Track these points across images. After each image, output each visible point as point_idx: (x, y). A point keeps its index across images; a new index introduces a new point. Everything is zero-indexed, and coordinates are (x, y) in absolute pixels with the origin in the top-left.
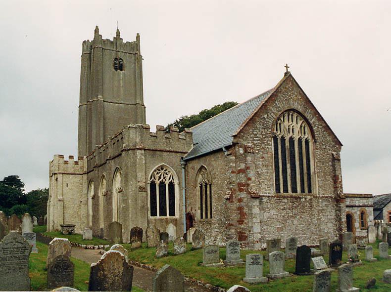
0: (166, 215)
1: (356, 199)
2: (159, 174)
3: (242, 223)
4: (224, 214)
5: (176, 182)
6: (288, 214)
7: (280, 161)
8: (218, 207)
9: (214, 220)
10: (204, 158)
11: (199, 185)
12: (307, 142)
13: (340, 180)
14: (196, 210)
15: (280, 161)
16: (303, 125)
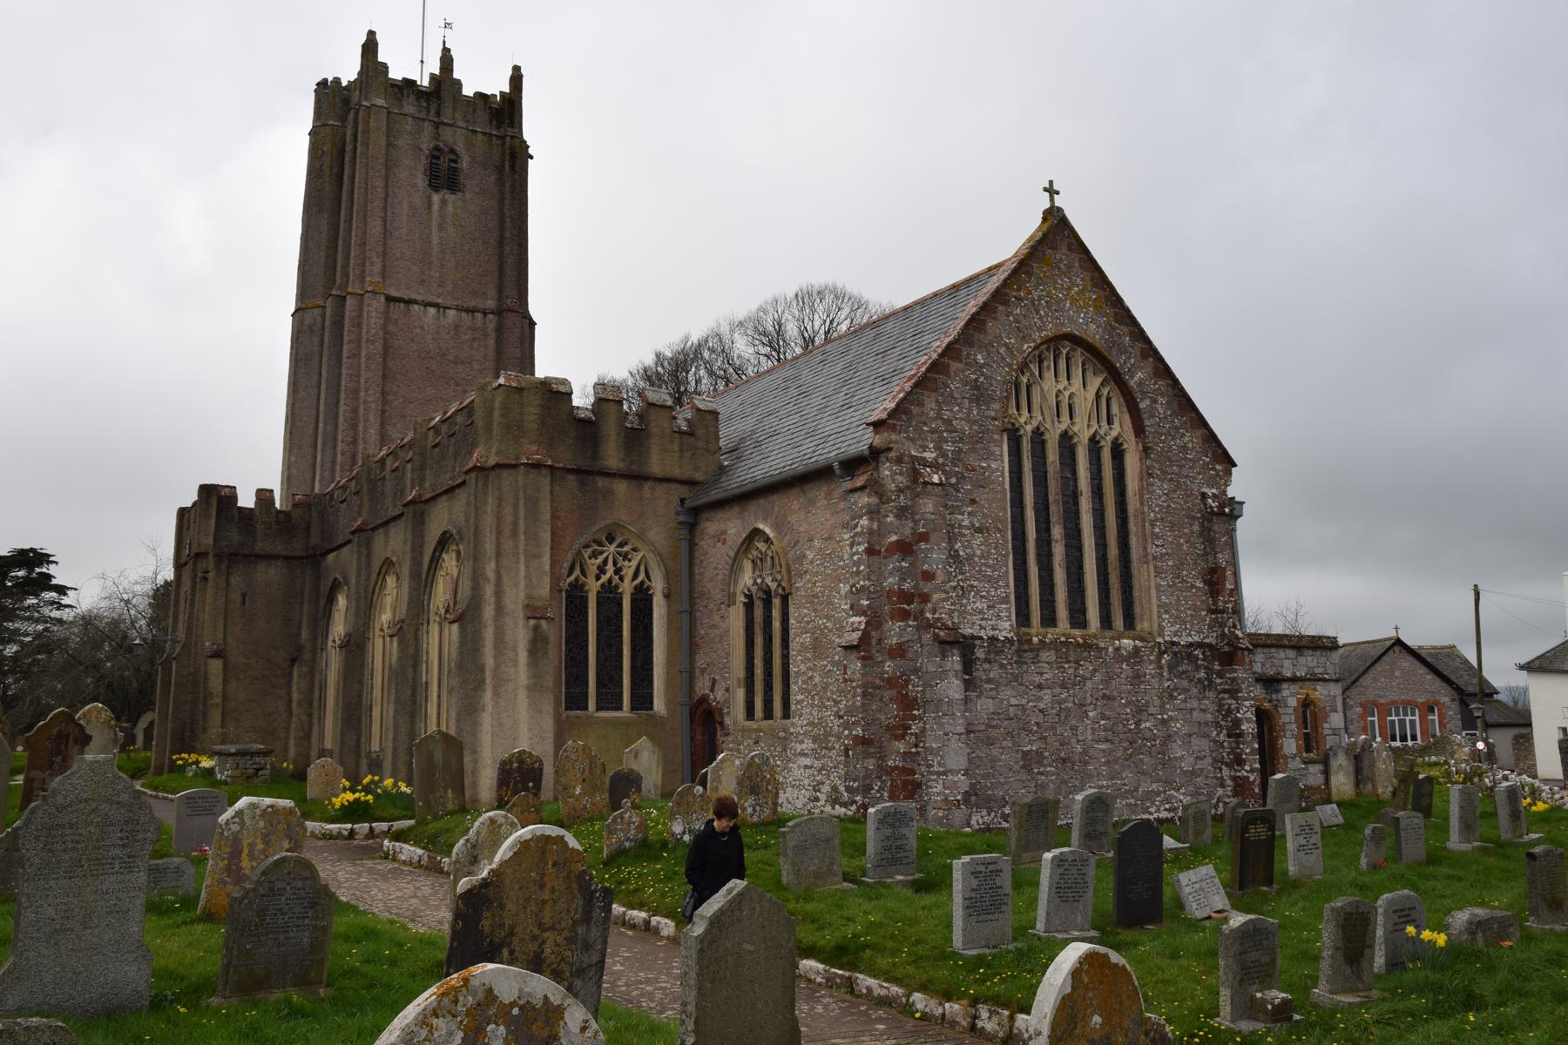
0: (620, 708)
1: (1282, 654)
2: (601, 559)
3: (903, 737)
4: (836, 702)
5: (658, 585)
6: (1060, 703)
7: (1030, 515)
8: (811, 678)
9: (798, 724)
10: (762, 501)
11: (743, 599)
12: (1118, 452)
13: (1229, 586)
14: (727, 690)
15: (1030, 515)
16: (1105, 392)
